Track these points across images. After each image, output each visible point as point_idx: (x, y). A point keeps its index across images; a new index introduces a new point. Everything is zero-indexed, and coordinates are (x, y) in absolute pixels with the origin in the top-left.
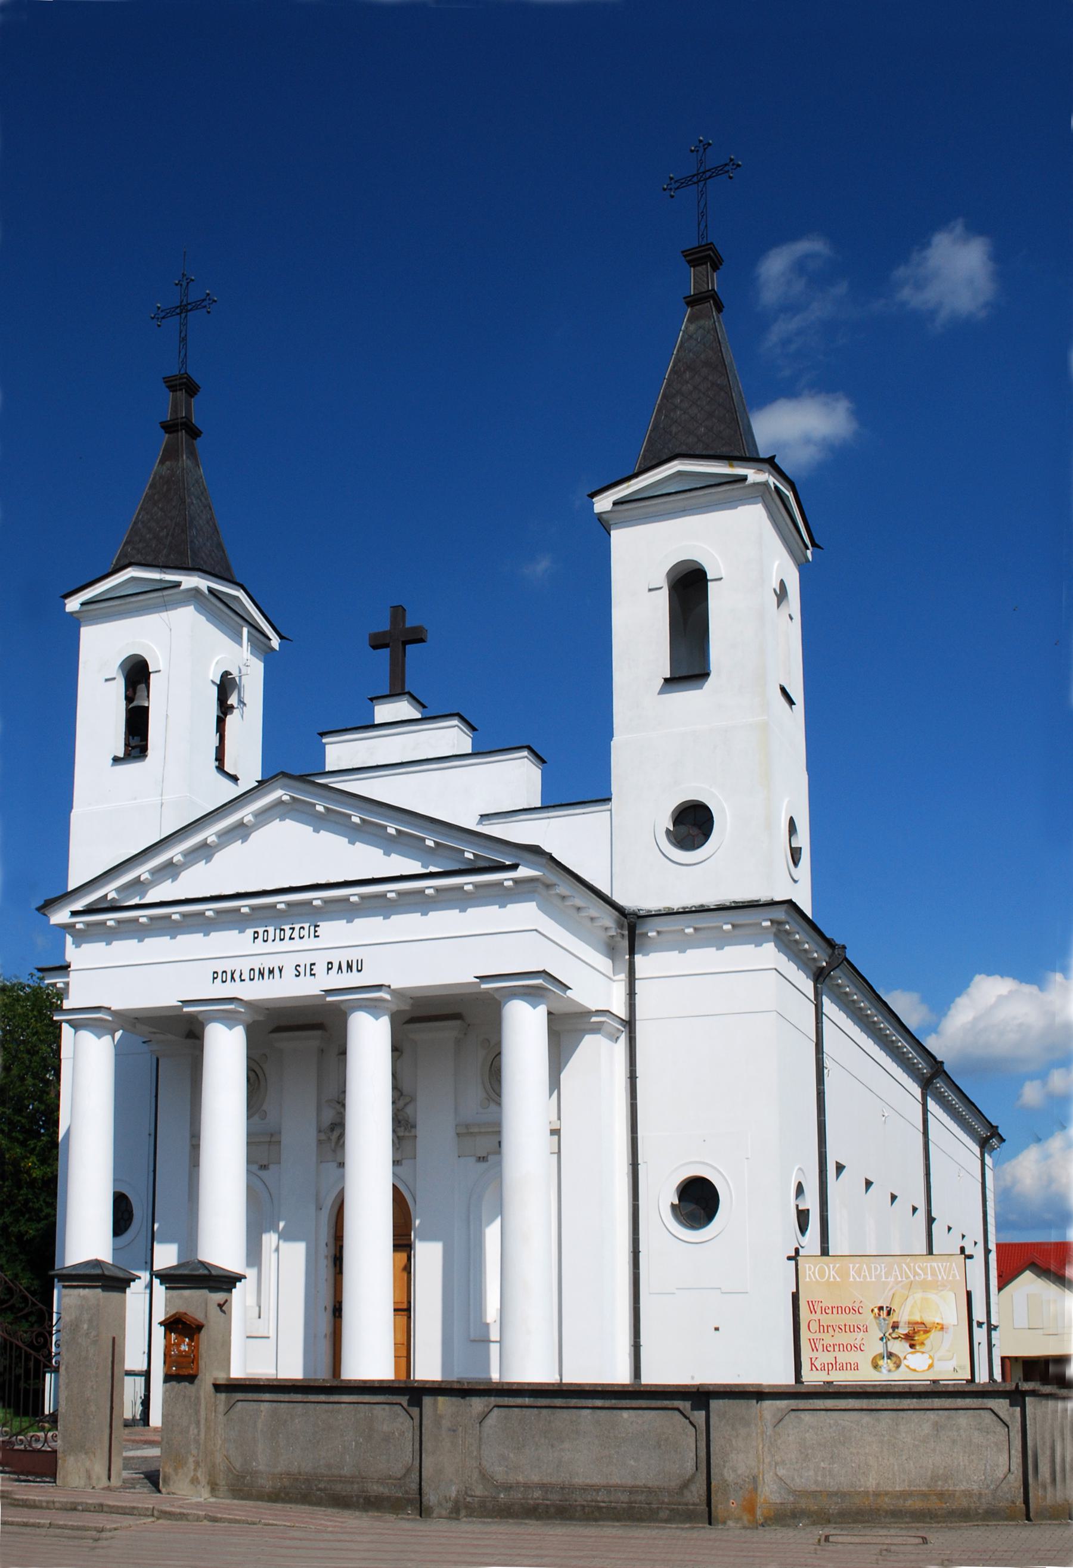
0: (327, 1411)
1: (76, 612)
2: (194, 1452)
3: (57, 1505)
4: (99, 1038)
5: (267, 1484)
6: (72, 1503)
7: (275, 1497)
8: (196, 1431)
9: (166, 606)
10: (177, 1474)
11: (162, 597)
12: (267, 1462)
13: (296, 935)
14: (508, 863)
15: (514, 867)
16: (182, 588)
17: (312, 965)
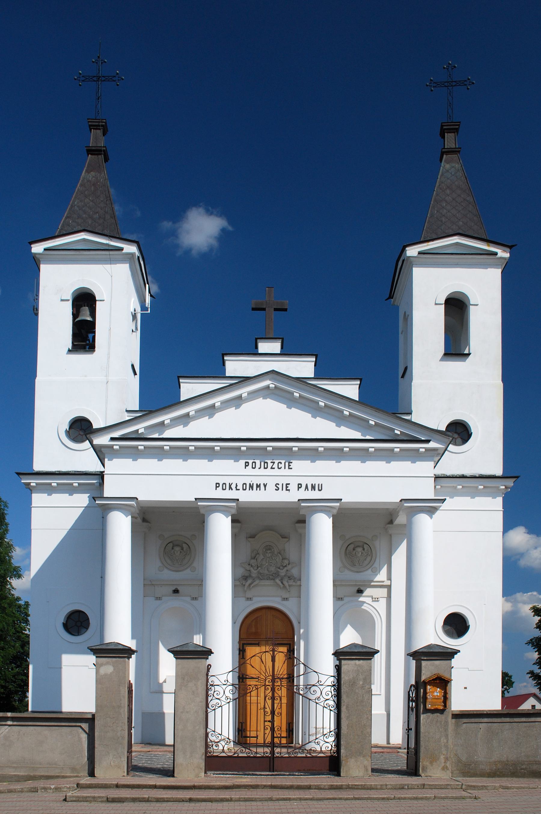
0: (525, 727)
1: (39, 254)
2: (444, 752)
3: (389, 787)
5: (487, 769)
7: (493, 774)
8: (445, 741)
10: (432, 766)
11: (109, 255)
12: (482, 756)
13: (275, 466)
14: (423, 439)
15: (428, 441)
16: (123, 251)
17: (287, 484)
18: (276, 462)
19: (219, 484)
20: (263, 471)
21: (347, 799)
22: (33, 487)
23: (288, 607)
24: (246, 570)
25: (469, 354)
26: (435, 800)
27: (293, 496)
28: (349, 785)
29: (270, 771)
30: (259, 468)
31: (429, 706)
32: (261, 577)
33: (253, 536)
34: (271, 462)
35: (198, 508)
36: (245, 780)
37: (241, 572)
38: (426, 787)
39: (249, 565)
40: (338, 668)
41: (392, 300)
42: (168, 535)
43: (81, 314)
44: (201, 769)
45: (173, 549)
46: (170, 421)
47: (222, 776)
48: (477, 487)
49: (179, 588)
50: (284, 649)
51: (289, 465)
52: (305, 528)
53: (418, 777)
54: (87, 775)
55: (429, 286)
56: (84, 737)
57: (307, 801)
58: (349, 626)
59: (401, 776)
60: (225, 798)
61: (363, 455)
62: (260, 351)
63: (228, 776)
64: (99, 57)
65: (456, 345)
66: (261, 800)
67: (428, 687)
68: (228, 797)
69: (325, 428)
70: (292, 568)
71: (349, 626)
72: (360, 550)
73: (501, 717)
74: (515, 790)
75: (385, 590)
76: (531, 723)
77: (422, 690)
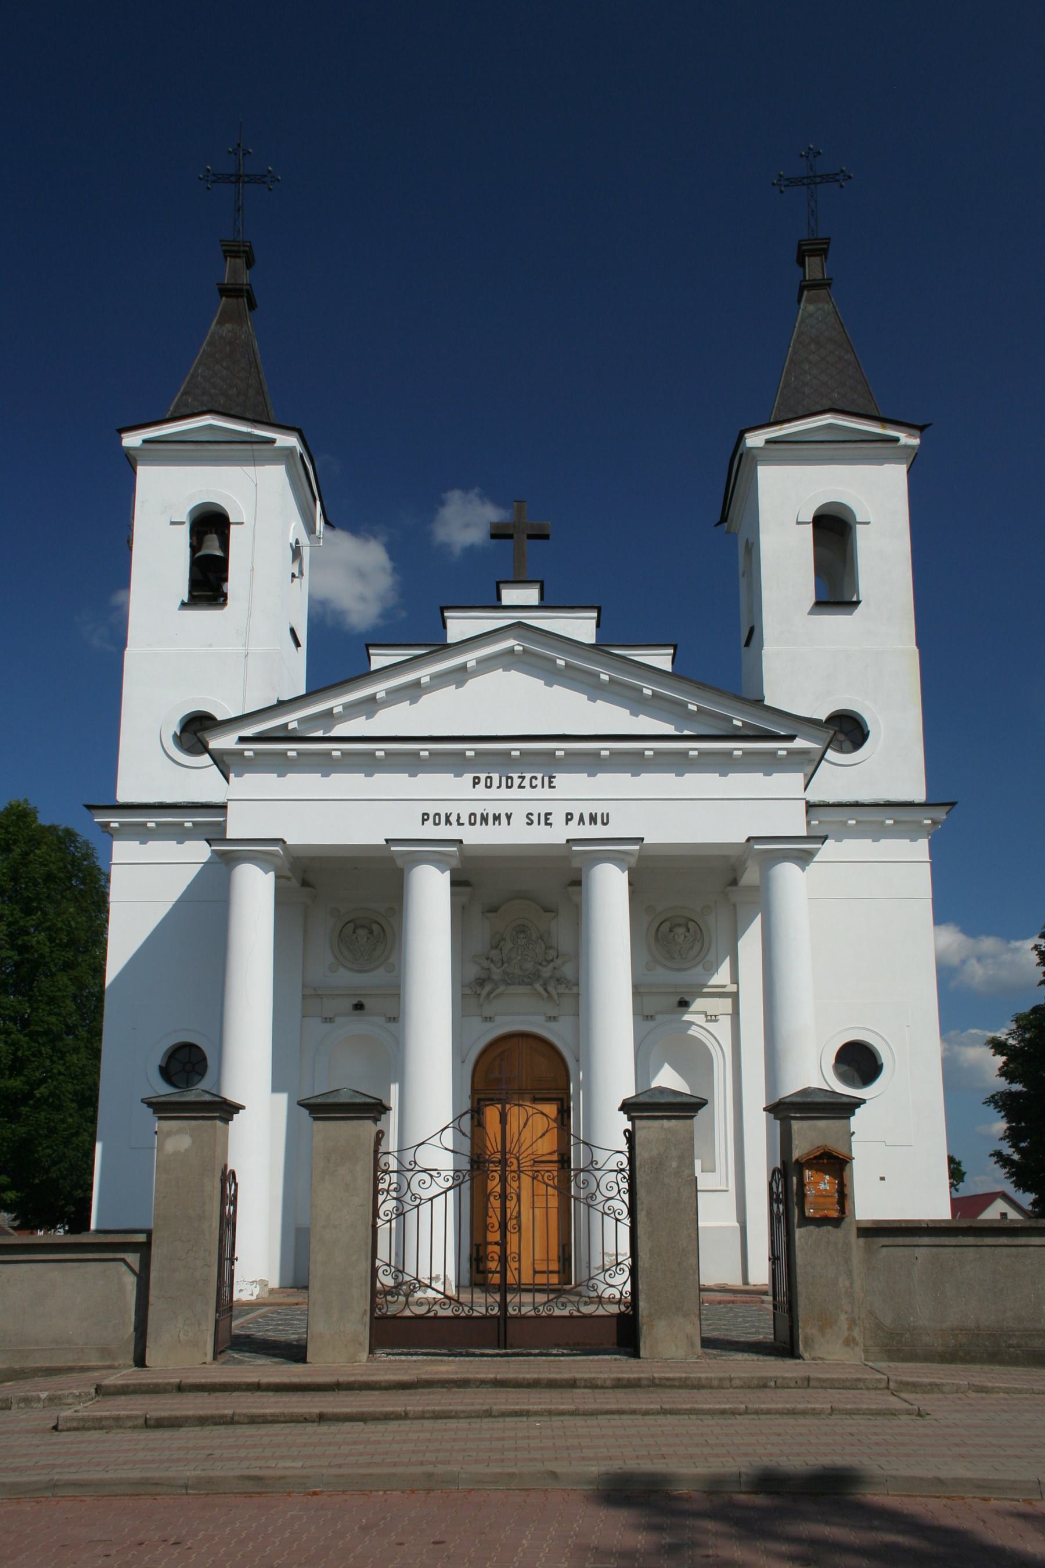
1: (135, 449)
3: (736, 1383)
4: (266, 873)
6: (759, 1378)
7: (949, 1357)
8: (847, 1283)
9: (255, 461)
11: (253, 451)
13: (526, 783)
15: (791, 738)
17: (547, 814)
18: (528, 776)
19: (427, 815)
20: (504, 793)
21: (646, 1413)
22: (115, 829)
23: (557, 1034)
24: (483, 968)
25: (858, 603)
26: (834, 1417)
27: (558, 834)
28: (654, 1378)
29: (499, 1347)
30: (498, 787)
31: (810, 1212)
32: (509, 980)
33: (493, 910)
34: (519, 777)
35: (391, 858)
36: (443, 1368)
37: (473, 971)
38: (812, 1384)
39: (487, 959)
40: (631, 1137)
41: (726, 524)
42: (343, 907)
43: (204, 546)
44: (360, 1344)
45: (354, 932)
46: (344, 708)
47: (403, 1358)
48: (883, 822)
49: (364, 1001)
50: (551, 1109)
51: (550, 782)
52: (580, 893)
53: (798, 1361)
54: (132, 1363)
55: (785, 496)
56: (130, 1282)
57: (562, 1418)
58: (666, 1065)
59: (761, 1358)
60: (392, 1413)
61: (680, 763)
62: (505, 602)
63: (415, 1358)
64: (239, 145)
65: (835, 591)
66: (469, 1415)
67: (809, 1173)
68: (399, 1409)
69: (611, 717)
70: (564, 963)
71: (666, 1065)
72: (681, 931)
73: (956, 1236)
74: (1002, 1395)
75: (728, 1002)
76: (1020, 1249)
77: (795, 1179)
